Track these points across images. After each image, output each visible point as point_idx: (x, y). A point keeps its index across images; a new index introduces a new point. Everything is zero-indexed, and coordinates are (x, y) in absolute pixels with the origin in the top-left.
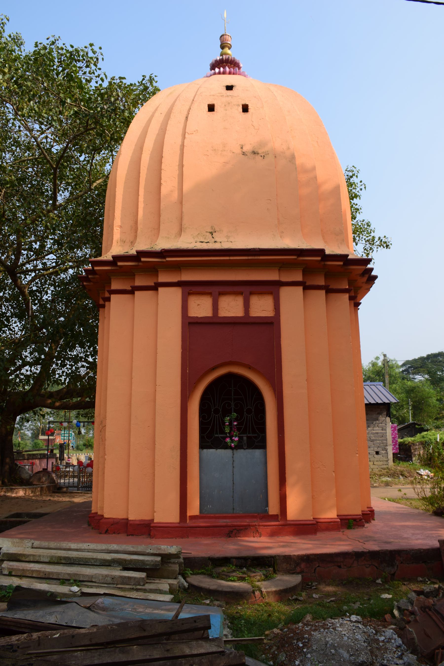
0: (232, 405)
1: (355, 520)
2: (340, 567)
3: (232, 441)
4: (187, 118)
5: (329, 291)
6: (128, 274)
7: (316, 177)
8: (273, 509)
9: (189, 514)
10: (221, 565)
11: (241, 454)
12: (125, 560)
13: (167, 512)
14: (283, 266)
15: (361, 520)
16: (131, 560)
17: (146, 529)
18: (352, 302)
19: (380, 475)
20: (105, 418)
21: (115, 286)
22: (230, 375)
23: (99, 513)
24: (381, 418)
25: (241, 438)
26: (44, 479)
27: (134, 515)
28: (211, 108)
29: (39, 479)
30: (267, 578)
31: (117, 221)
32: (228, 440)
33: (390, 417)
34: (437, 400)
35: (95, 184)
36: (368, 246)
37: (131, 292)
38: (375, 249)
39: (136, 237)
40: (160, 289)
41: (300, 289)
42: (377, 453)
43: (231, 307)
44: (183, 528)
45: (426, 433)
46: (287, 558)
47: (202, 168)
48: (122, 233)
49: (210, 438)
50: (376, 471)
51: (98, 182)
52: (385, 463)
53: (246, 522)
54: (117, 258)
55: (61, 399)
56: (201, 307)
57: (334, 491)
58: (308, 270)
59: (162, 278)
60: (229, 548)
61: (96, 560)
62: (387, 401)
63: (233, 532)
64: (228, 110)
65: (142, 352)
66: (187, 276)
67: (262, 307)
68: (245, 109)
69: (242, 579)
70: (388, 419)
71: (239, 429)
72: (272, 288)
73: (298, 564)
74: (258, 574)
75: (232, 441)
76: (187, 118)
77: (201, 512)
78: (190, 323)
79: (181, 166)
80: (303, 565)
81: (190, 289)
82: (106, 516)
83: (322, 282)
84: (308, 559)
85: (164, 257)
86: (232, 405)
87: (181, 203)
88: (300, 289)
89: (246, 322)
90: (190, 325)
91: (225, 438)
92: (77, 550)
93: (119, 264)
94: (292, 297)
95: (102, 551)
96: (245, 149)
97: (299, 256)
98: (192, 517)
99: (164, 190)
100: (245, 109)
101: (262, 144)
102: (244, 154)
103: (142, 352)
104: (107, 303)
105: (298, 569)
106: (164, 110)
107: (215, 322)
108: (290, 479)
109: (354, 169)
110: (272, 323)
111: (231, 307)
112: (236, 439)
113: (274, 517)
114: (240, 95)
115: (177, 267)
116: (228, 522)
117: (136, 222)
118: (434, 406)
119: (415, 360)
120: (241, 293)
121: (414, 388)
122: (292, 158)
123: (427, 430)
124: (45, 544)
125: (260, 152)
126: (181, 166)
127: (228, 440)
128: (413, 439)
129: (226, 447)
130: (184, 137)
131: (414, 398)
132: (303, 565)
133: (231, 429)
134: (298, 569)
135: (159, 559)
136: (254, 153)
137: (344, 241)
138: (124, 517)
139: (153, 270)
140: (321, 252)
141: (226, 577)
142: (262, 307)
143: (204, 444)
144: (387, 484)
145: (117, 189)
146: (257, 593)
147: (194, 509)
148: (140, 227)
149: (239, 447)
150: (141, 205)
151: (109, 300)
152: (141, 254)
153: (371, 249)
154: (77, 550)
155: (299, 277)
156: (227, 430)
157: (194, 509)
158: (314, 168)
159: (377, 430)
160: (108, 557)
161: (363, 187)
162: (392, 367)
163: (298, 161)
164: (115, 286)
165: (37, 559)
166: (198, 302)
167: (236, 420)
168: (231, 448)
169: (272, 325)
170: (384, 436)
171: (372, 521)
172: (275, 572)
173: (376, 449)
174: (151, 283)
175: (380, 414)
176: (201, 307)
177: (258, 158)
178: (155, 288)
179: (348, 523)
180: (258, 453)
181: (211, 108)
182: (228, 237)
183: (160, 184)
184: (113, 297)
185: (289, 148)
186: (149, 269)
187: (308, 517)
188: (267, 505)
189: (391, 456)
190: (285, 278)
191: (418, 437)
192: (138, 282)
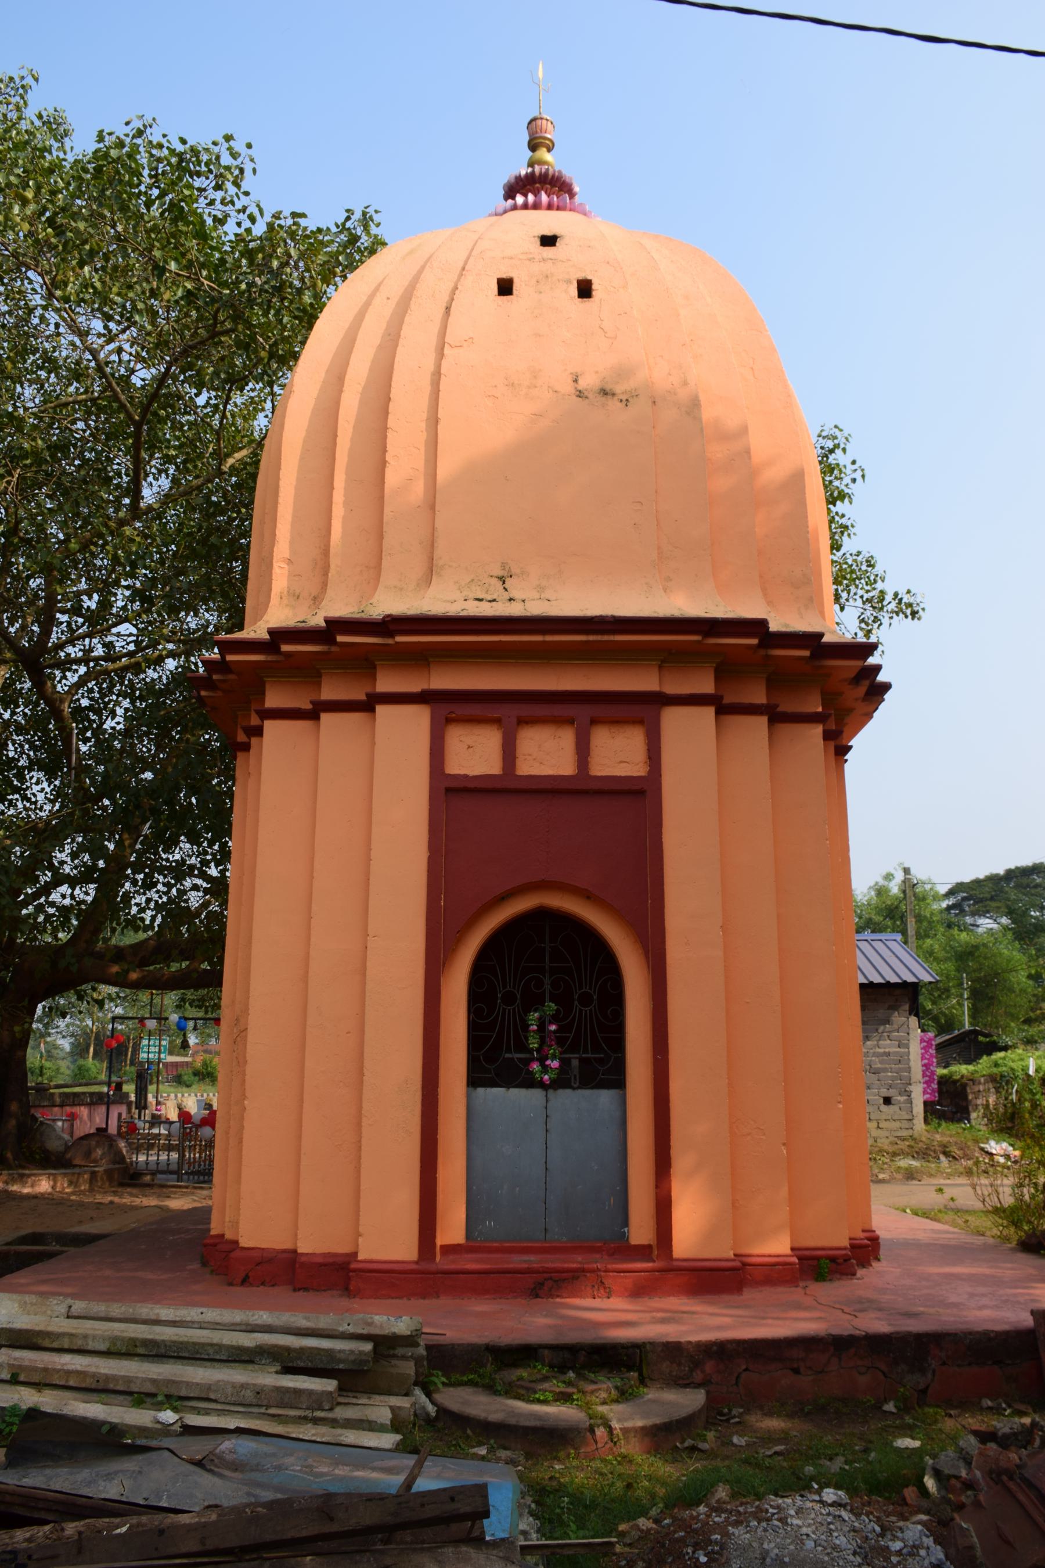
0: (545, 985)
1: (833, 1259)
2: (796, 1371)
3: (545, 1069)
4: (448, 309)
5: (777, 717)
6: (306, 672)
7: (748, 452)
8: (640, 1230)
9: (443, 1238)
10: (515, 1365)
11: (567, 1100)
12: (288, 1349)
13: (388, 1236)
14: (669, 658)
15: (847, 1259)
16: (302, 1350)
17: (339, 1275)
18: (832, 745)
19: (895, 1154)
20: (246, 1010)
21: (273, 699)
22: (541, 914)
23: (228, 1236)
24: (898, 1018)
25: (565, 1063)
26: (99, 1152)
27: (312, 1242)
28: (505, 287)
29: (88, 1154)
30: (624, 1395)
31: (282, 549)
32: (536, 1067)
33: (917, 1015)
34: (1030, 977)
35: (230, 461)
36: (869, 613)
37: (312, 714)
38: (885, 621)
39: (324, 585)
40: (380, 709)
41: (708, 713)
42: (887, 1101)
43: (546, 753)
44: (427, 1275)
45: (1002, 1054)
46: (673, 1350)
47: (481, 426)
48: (293, 576)
49: (494, 1060)
50: (884, 1143)
51: (238, 455)
52: (905, 1124)
53: (575, 1261)
54: (279, 635)
55: (143, 963)
56: (475, 753)
57: (784, 1192)
58: (727, 669)
59: (386, 683)
60: (533, 1323)
61: (219, 1347)
62: (911, 979)
63: (544, 1286)
64: (546, 292)
65: (335, 860)
66: (443, 680)
67: (617, 754)
68: (585, 290)
69: (564, 1398)
70: (913, 1021)
71: (560, 1042)
72: (642, 710)
73: (696, 1364)
74: (604, 1387)
75: (545, 1069)
76: (448, 309)
77: (468, 1237)
78: (448, 790)
79: (434, 421)
80: (709, 1366)
81: (450, 708)
82: (244, 1243)
83: (759, 697)
84: (722, 1352)
85: (391, 634)
86: (545, 985)
87: (432, 507)
88: (710, 712)
89: (581, 790)
90: (450, 794)
91: (528, 1062)
92: (173, 1324)
93: (285, 648)
94: (689, 736)
95: (233, 1327)
96: (582, 384)
97: (707, 634)
98: (449, 1250)
99: (393, 478)
100: (585, 290)
101: (622, 372)
102: (580, 394)
103: (335, 860)
104: (254, 741)
105: (698, 1376)
106: (395, 289)
107: (507, 789)
108: (681, 1161)
109: (837, 433)
110: (641, 793)
111: (546, 753)
112: (555, 1064)
113: (643, 1252)
114: (572, 260)
115: (420, 659)
116: (532, 1260)
117: (326, 552)
118: (1023, 991)
119: (977, 882)
120: (569, 721)
121: (976, 947)
122: (694, 405)
123: (1005, 1048)
124: (99, 1308)
125: (618, 389)
126: (434, 421)
127: (536, 1067)
128: (971, 1068)
129: (530, 1082)
130: (440, 354)
131: (974, 971)
132: (709, 1366)
133: (542, 1042)
134: (698, 1376)
135: (368, 1347)
136: (604, 392)
137: (814, 601)
138: (288, 1246)
139: (364, 663)
140: (758, 626)
141: (526, 1393)
142: (617, 754)
143: (479, 1076)
144: (910, 1175)
145: (283, 474)
146: (600, 1432)
147: (452, 1229)
148: (334, 562)
149: (561, 1082)
150: (338, 511)
151: (259, 732)
152: (336, 626)
153: (876, 619)
154: (173, 1324)
155: (706, 685)
156: (534, 1043)
157: (452, 1229)
158: (744, 430)
159: (888, 1046)
160: (248, 1340)
161: (858, 475)
162: (924, 899)
163: (707, 414)
164: (273, 699)
165: (79, 1343)
166: (469, 740)
167: (555, 1019)
168: (541, 1085)
169: (641, 796)
170: (903, 1060)
171: (875, 1264)
172: (642, 1381)
173: (885, 1093)
174: (358, 694)
175: (894, 1008)
176: (475, 753)
177: (613, 404)
178: (368, 706)
179: (817, 1266)
180: (605, 1097)
181: (505, 287)
182: (541, 588)
183: (383, 463)
184: (269, 725)
185: (685, 383)
186: (354, 660)
187: (722, 1250)
188: (626, 1223)
189: (919, 1108)
190: (672, 688)
191: (984, 1065)
192: (329, 692)
